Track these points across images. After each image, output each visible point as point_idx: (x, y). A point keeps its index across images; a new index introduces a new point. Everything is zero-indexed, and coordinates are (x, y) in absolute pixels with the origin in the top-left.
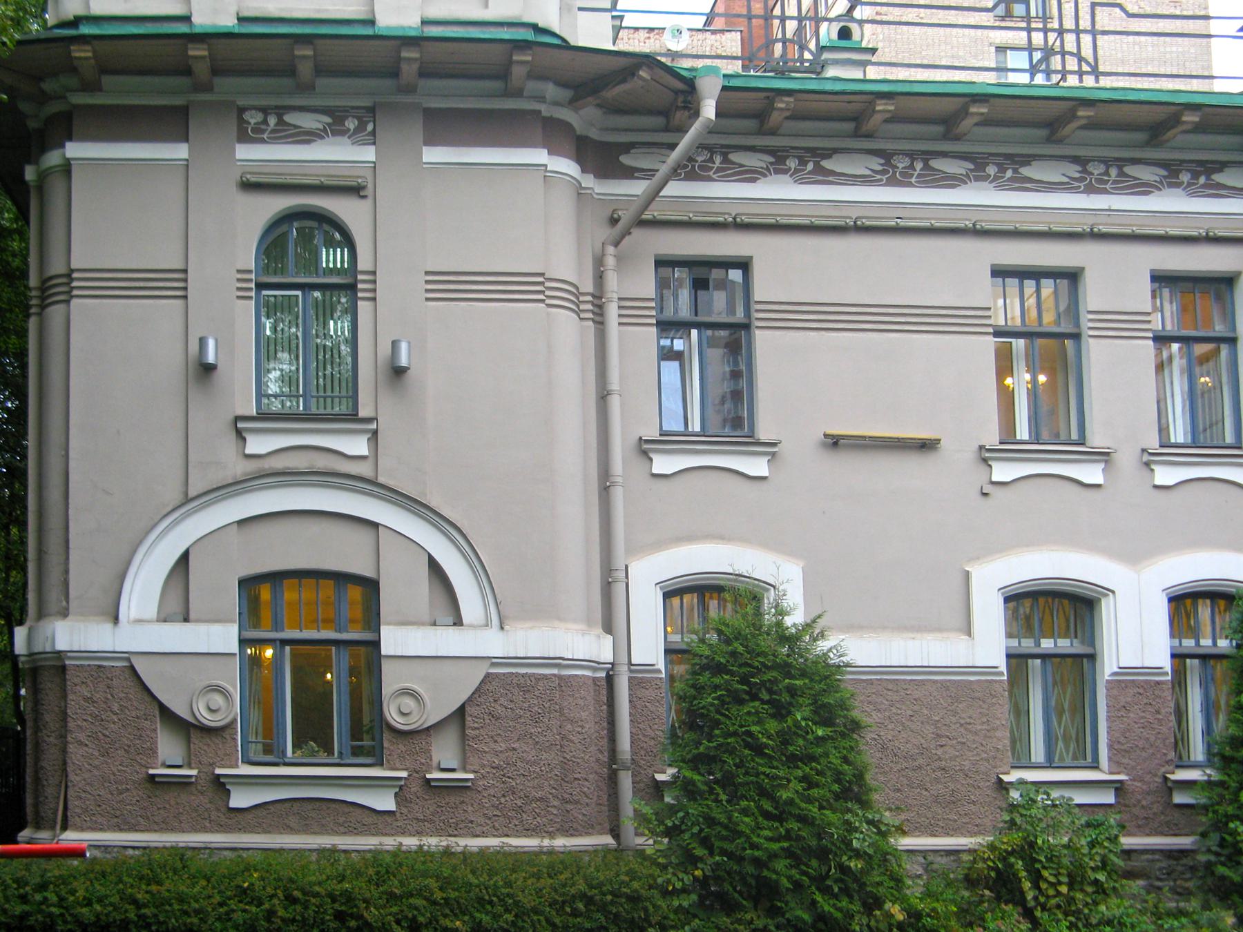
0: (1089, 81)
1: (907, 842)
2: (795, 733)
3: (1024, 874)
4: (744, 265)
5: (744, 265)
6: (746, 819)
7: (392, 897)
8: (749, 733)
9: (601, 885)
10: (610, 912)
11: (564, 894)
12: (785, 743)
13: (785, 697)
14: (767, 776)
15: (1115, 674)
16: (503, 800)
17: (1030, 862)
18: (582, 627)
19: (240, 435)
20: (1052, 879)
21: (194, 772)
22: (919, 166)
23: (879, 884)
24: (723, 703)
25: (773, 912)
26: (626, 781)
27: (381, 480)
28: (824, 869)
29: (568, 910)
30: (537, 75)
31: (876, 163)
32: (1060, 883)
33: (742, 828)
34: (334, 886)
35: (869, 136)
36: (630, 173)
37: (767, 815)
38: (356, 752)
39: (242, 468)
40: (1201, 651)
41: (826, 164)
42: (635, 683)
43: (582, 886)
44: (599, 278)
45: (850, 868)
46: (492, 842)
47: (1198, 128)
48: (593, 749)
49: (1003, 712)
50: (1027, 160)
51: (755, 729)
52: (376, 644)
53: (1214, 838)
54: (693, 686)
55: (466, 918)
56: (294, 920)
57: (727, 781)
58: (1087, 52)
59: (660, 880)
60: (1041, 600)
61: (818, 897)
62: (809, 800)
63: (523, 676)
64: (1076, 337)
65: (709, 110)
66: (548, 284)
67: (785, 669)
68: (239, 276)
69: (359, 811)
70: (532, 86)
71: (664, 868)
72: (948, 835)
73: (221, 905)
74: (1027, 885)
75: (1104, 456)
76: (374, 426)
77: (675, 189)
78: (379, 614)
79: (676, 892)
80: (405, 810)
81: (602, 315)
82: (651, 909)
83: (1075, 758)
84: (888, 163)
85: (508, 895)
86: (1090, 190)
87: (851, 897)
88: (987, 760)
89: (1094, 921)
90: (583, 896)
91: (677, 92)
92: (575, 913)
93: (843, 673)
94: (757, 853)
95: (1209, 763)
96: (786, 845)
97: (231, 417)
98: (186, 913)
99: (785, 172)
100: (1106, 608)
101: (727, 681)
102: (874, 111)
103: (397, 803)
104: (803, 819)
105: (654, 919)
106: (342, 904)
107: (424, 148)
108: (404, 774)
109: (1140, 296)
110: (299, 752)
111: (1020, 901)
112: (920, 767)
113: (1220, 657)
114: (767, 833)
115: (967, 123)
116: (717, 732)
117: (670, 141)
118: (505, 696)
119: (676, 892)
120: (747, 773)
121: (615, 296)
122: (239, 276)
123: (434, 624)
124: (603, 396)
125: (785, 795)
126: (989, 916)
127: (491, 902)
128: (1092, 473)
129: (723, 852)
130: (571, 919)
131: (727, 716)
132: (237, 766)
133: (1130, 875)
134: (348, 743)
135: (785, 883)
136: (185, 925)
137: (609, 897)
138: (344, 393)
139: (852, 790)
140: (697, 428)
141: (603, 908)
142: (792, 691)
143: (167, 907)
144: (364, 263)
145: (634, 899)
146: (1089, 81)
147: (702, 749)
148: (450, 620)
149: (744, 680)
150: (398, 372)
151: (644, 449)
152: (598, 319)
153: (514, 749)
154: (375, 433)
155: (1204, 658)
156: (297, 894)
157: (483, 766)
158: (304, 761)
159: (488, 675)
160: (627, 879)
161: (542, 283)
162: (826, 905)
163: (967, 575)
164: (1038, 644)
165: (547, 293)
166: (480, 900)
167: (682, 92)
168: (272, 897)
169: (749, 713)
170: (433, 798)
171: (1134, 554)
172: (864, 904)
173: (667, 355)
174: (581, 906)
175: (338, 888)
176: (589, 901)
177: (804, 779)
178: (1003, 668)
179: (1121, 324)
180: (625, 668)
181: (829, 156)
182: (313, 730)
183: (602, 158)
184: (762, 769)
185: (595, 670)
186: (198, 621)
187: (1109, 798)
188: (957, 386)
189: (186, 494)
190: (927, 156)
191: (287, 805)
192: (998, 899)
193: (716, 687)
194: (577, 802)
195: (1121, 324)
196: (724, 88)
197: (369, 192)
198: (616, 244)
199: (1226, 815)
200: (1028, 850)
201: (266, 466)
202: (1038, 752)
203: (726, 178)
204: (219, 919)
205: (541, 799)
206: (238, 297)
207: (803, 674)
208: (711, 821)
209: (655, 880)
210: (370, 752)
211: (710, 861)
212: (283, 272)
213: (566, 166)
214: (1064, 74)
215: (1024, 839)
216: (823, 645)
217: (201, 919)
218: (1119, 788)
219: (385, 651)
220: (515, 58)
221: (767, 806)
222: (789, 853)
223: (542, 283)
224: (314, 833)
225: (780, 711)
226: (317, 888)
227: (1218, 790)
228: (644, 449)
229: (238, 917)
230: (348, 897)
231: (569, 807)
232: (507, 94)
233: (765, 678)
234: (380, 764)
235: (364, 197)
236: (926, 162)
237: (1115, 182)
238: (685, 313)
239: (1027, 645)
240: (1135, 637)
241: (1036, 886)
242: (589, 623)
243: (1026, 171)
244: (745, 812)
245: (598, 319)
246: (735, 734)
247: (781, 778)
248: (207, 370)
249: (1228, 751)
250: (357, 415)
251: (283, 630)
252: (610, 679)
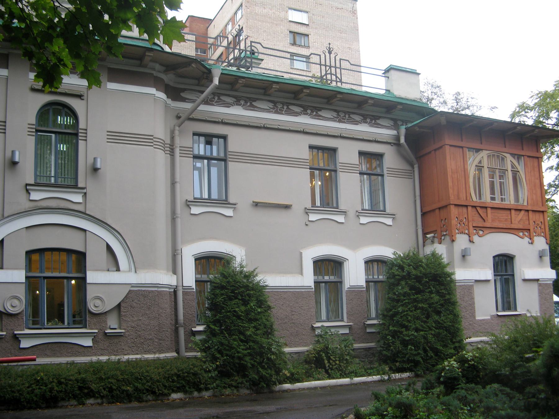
0: (339, 84)
1: (287, 350)
2: (251, 311)
3: (325, 358)
4: (225, 138)
5: (225, 138)
6: (235, 343)
7: (101, 379)
8: (235, 311)
9: (182, 370)
10: (186, 380)
11: (168, 374)
12: (247, 314)
13: (247, 298)
14: (242, 326)
15: (349, 288)
16: (136, 340)
17: (327, 353)
18: (165, 272)
19: (27, 191)
20: (334, 359)
21: (4, 333)
22: (285, 107)
23: (280, 364)
24: (225, 300)
25: (244, 376)
26: (182, 331)
27: (87, 212)
28: (262, 359)
29: (171, 380)
30: (154, 61)
31: (271, 105)
32: (336, 360)
33: (234, 346)
34: (77, 376)
35: (269, 95)
36: (184, 100)
37: (242, 341)
38: (75, 322)
39: (28, 205)
40: (374, 280)
41: (254, 103)
42: (185, 294)
43: (176, 371)
44: (172, 138)
45: (271, 358)
46: (138, 356)
47: (373, 105)
48: (169, 319)
49: (313, 302)
50: (320, 109)
51: (237, 309)
52: (84, 279)
53: (382, 342)
54: (213, 294)
55: (132, 386)
56: (61, 391)
57: (227, 329)
58: (339, 76)
59: (204, 367)
61: (260, 369)
62: (257, 335)
63: (144, 291)
64: (335, 171)
65: (216, 81)
66: (155, 140)
67: (247, 287)
68: (29, 126)
69: (77, 347)
70: (151, 64)
71: (205, 362)
72: (295, 347)
73: (28, 387)
74: (326, 362)
75: (344, 213)
76: (85, 191)
77: (202, 107)
78: (85, 266)
79: (210, 371)
80: (96, 346)
81: (173, 152)
82: (202, 378)
83: (335, 318)
84: (275, 105)
85: (147, 376)
86: (340, 121)
87: (271, 369)
88: (308, 319)
89: (347, 373)
90: (176, 374)
91: (204, 73)
92: (173, 381)
93: (265, 289)
94: (240, 355)
95: (377, 318)
96: (249, 351)
97: (24, 184)
98: (13, 392)
99: (240, 105)
100: (346, 265)
101: (226, 292)
102: (272, 87)
103: (93, 343)
104: (254, 342)
105: (203, 381)
106: (81, 383)
107: (108, 83)
108: (96, 331)
109: (355, 159)
110: (50, 324)
111: (324, 367)
112: (286, 323)
113: (382, 282)
114: (242, 347)
115: (302, 95)
116: (223, 311)
117: (202, 90)
118: (138, 299)
119: (210, 371)
120: (234, 326)
121: (179, 146)
122: (29, 126)
123: (108, 270)
124: (173, 183)
125: (248, 333)
126: (314, 373)
127: (140, 379)
128: (340, 218)
129: (227, 355)
130: (172, 383)
131: (226, 305)
132: (24, 330)
133: (355, 357)
134: (72, 319)
135: (249, 365)
136: (13, 397)
137: (186, 374)
138: (73, 177)
139: (269, 332)
140: (207, 197)
141: (184, 378)
142: (249, 295)
143: (5, 390)
144: (82, 125)
145: (195, 374)
146: (339, 84)
147: (218, 317)
148: (115, 269)
149: (233, 292)
150: (95, 170)
151: (188, 204)
152: (171, 154)
153: (140, 320)
154: (85, 193)
155: (375, 282)
156: (62, 380)
157: (128, 327)
158: (53, 327)
159: (130, 291)
160: (192, 367)
161: (152, 139)
162: (263, 372)
163: (301, 253)
164: (324, 278)
165: (154, 143)
166: (137, 379)
167: (207, 73)
168: (51, 382)
169: (234, 304)
170: (107, 339)
171: (354, 246)
172: (275, 371)
173: (195, 168)
174: (175, 378)
175: (80, 377)
176: (178, 376)
177: (254, 327)
178: (313, 287)
179: (349, 168)
180: (181, 288)
181: (255, 101)
182: (56, 315)
183: (174, 93)
184: (240, 324)
185: (170, 288)
186: (7, 269)
187: (347, 331)
188: (297, 186)
189: (3, 215)
190: (288, 104)
191: (46, 345)
192: (317, 367)
193: (222, 294)
194: (164, 340)
195: (349, 168)
196: (222, 74)
197: (85, 97)
198: (179, 127)
199: (385, 334)
200: (326, 349)
201: (39, 205)
202: (324, 317)
203: (219, 105)
204: (28, 393)
205: (151, 339)
206: (29, 135)
207: (253, 290)
208: (222, 344)
209: (202, 367)
210: (80, 322)
211: (222, 359)
212: (48, 127)
213: (162, 95)
214: (332, 81)
215: (325, 346)
216: (258, 278)
217: (20, 394)
218: (350, 327)
219: (89, 281)
220: (147, 54)
221: (242, 337)
222: (250, 354)
223: (152, 139)
224: (58, 357)
225: (245, 303)
226: (71, 378)
227: (383, 326)
228: (188, 204)
229: (37, 391)
230: (84, 381)
231: (161, 342)
232: (140, 66)
233: (240, 291)
234: (85, 327)
235: (83, 99)
238: (202, 153)
239: (320, 278)
240: (355, 276)
241: (329, 362)
242: (168, 270)
243: (320, 113)
244: (234, 340)
245: (171, 154)
246: (230, 312)
247: (246, 327)
248: (14, 164)
249: (385, 313)
250: (77, 186)
251: (44, 273)
252: (175, 292)
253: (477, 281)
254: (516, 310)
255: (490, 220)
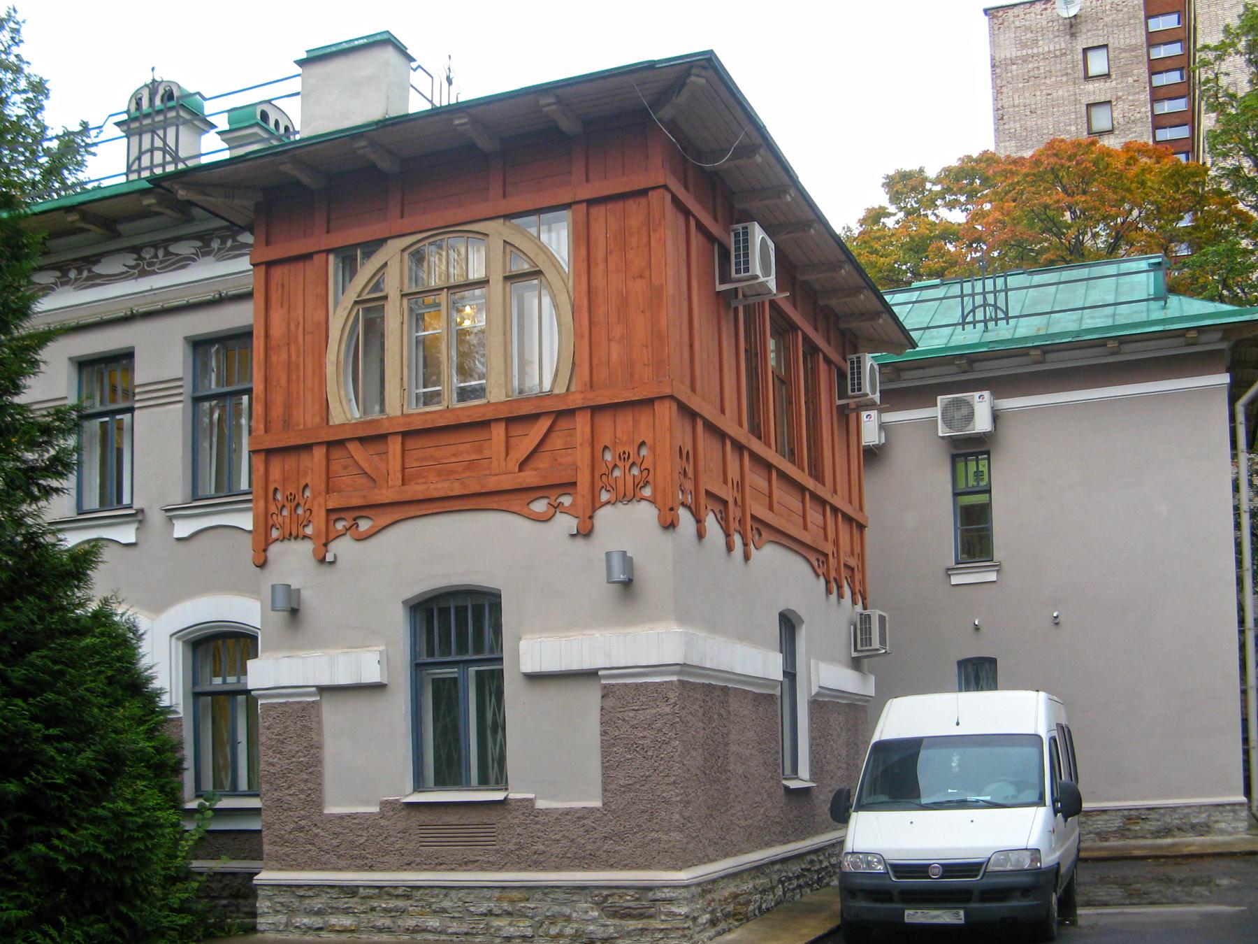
50: (95, 259)
60: (242, 640)
195: (163, 392)
236: (166, 248)
237: (162, 262)
243: (97, 269)
253: (322, 690)
254: (501, 781)
255: (395, 478)
